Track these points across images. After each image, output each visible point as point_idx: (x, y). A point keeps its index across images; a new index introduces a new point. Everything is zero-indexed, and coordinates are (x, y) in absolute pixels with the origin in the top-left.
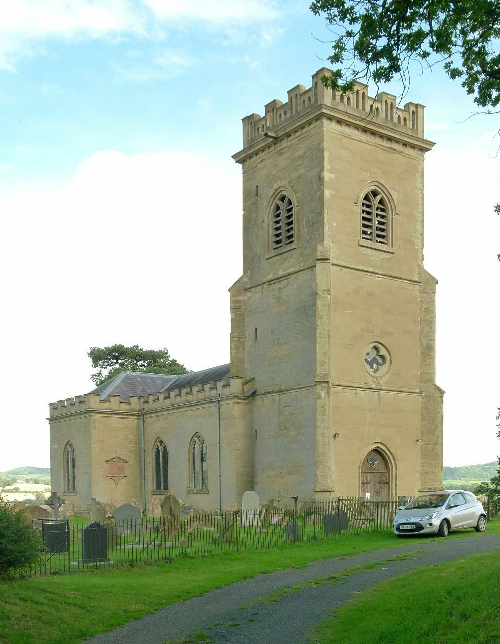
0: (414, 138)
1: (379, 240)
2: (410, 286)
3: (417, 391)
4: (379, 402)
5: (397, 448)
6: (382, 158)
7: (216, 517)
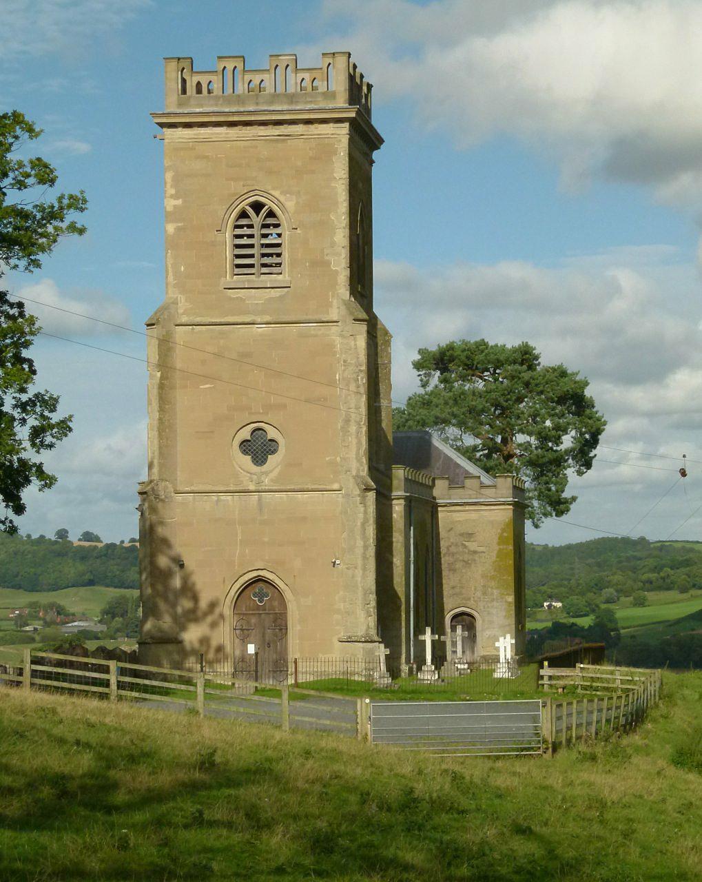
0: (337, 110)
1: (265, 270)
2: (320, 330)
3: (336, 486)
4: (261, 510)
5: (294, 576)
6: (266, 153)
7: (315, 663)
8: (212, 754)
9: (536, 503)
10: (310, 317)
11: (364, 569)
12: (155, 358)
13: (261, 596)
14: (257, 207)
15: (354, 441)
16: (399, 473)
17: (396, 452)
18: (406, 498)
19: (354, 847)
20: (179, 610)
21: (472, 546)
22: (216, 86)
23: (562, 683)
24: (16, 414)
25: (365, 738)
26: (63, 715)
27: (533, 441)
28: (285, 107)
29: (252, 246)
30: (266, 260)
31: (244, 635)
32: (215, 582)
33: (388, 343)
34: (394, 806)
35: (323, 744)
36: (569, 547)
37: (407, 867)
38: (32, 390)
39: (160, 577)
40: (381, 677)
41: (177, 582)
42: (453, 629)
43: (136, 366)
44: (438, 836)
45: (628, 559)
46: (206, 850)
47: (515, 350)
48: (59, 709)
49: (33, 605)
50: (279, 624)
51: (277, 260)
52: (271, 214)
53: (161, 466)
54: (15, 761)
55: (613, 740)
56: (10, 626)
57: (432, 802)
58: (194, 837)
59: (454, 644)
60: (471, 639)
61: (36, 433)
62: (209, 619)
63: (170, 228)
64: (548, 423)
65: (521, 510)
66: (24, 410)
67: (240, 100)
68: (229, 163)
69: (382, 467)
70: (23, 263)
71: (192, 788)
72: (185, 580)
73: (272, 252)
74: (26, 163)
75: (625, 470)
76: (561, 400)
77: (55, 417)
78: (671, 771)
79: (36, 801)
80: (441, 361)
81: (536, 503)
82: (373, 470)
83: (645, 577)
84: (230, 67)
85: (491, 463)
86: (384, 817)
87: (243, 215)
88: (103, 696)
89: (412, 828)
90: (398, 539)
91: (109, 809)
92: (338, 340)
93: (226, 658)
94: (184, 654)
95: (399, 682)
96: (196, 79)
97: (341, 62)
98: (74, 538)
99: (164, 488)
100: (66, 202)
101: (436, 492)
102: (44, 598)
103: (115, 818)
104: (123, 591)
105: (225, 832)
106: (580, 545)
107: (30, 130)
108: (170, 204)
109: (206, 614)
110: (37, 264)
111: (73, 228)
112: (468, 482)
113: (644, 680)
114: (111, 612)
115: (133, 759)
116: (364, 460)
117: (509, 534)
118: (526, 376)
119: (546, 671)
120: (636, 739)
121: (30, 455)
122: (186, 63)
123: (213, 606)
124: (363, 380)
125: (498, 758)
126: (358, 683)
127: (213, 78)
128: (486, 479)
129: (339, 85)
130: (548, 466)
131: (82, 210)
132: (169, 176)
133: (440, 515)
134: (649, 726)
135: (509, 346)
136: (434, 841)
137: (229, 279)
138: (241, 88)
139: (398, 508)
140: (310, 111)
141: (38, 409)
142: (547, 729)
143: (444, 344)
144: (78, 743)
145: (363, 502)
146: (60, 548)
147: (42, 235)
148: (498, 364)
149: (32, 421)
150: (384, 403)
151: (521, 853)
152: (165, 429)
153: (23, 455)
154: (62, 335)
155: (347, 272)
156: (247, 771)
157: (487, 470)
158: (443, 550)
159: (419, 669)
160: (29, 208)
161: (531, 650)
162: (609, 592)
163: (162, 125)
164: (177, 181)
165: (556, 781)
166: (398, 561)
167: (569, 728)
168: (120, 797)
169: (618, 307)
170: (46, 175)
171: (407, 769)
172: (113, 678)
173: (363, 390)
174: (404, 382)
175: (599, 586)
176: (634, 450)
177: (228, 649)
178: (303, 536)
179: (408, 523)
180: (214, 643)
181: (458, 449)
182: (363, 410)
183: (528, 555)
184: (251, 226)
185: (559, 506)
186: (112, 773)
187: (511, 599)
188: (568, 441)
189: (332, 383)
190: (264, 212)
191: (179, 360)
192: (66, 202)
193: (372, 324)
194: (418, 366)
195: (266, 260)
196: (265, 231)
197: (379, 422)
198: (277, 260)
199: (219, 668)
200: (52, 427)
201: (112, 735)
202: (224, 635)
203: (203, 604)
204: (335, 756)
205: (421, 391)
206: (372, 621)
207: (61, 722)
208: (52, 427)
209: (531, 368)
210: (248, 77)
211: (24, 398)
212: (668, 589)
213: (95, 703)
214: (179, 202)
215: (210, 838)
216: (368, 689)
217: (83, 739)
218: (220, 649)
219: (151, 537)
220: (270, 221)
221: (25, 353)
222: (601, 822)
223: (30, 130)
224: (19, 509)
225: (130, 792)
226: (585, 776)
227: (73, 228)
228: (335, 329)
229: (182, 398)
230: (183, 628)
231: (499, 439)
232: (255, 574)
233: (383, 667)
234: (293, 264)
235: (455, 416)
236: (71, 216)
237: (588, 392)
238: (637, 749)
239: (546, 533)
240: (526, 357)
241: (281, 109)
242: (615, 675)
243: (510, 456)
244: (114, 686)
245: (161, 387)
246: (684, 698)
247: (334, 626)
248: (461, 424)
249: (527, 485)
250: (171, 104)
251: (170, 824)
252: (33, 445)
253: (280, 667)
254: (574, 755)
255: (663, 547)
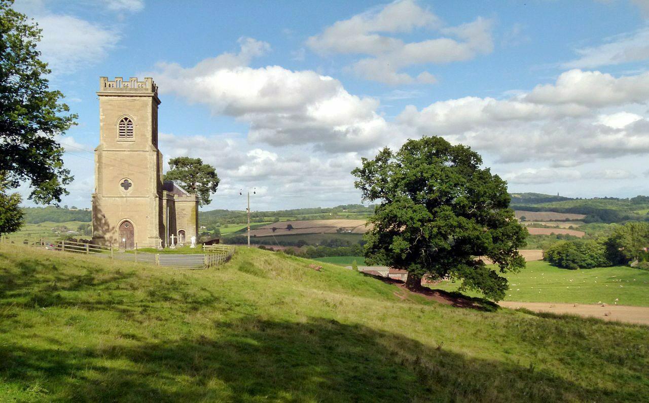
3: (148, 196)
8: (119, 270)
9: (201, 201)
10: (141, 150)
11: (155, 218)
12: (97, 160)
13: (127, 225)
14: (126, 119)
15: (153, 184)
16: (165, 193)
17: (164, 187)
18: (167, 200)
19: (160, 295)
20: (104, 229)
21: (184, 212)
22: (115, 85)
23: (208, 249)
24: (58, 174)
25: (157, 265)
26: (76, 259)
27: (201, 184)
28: (134, 92)
29: (124, 130)
30: (128, 134)
31: (122, 237)
32: (114, 221)
33: (162, 157)
34: (170, 283)
35: (147, 266)
36: (208, 212)
37: (175, 300)
38: (63, 168)
39: (98, 220)
40: (160, 247)
41: (103, 221)
42: (179, 234)
43: (91, 161)
44: (182, 291)
45: (223, 215)
46: (121, 296)
47: (196, 160)
48: (74, 257)
49: (58, 226)
50: (132, 233)
51: (132, 134)
52: (130, 121)
53: (98, 190)
54: (65, 272)
55: (223, 264)
56: (51, 232)
57: (179, 282)
58: (116, 293)
59: (179, 239)
60: (184, 237)
61: (64, 180)
62: (112, 232)
63: (101, 124)
64: (205, 180)
65: (197, 203)
66: (61, 174)
67: (121, 89)
68: (119, 107)
69: (160, 191)
70: (61, 133)
71: (115, 279)
72: (106, 221)
73: (130, 131)
74: (61, 105)
75: (226, 191)
76: (208, 174)
77: (69, 176)
78: (239, 272)
79: (73, 283)
80: (176, 162)
81: (201, 201)
82: (158, 192)
83: (227, 220)
84: (119, 80)
85: (189, 190)
86: (167, 286)
87: (122, 121)
88: (85, 253)
89: (176, 289)
90: (164, 210)
91: (94, 285)
92: (148, 156)
93: (117, 242)
94: (105, 241)
95: (165, 249)
96: (109, 83)
97: (150, 80)
98: (70, 208)
99: (99, 196)
100: (72, 116)
101: (174, 198)
102: (61, 224)
103: (96, 287)
104: (83, 223)
105: (126, 291)
106: (211, 211)
107: (62, 96)
108: (101, 117)
109: (111, 230)
110: (64, 133)
111: (74, 123)
112: (183, 195)
113: (230, 248)
114: (80, 228)
115: (97, 271)
116: (156, 189)
117: (194, 210)
118: (199, 167)
119: (205, 246)
120: (228, 264)
121: (62, 186)
122: (106, 79)
123: (113, 228)
124: (155, 167)
125: (194, 269)
126: (154, 249)
127: (114, 83)
128: (188, 194)
129: (149, 87)
130: (205, 191)
131: (77, 118)
132: (101, 110)
133: (176, 204)
134: (232, 260)
135: (194, 159)
136: (181, 292)
137: (118, 139)
138: (122, 86)
139: (165, 202)
140: (121, 93)
141: (64, 173)
142: (206, 262)
143: (177, 158)
144: (82, 267)
145: (155, 200)
146: (66, 211)
147: (65, 125)
148: (192, 164)
149: (63, 177)
150: (161, 173)
151: (204, 295)
152: (100, 180)
153: (61, 186)
154: (74, 152)
155: (151, 138)
156: (128, 274)
157: (188, 192)
158: (176, 214)
159: (170, 245)
160: (61, 117)
161: (198, 242)
162: (218, 224)
163: (99, 95)
164: (103, 111)
165: (210, 276)
166: (164, 216)
167: (212, 261)
168: (95, 282)
169: (228, 149)
170: (67, 108)
171: (171, 273)
172: (88, 249)
173: (155, 170)
174: (166, 168)
175: (215, 222)
176: (227, 186)
177: (118, 240)
178: (141, 208)
179: (167, 206)
180: (114, 238)
181: (180, 186)
182: (155, 176)
183: (199, 214)
184: (124, 124)
185: (207, 202)
186: (92, 275)
187: (195, 227)
188: (210, 185)
189: (147, 168)
190: (128, 121)
191: (104, 160)
192: (72, 116)
193: (158, 152)
194: (169, 163)
195: (128, 134)
196: (128, 126)
197: (160, 179)
198: (132, 134)
199: (115, 245)
200: (68, 178)
201: (90, 264)
202: (117, 236)
203: (111, 227)
204: (151, 270)
205: (171, 170)
206: (157, 232)
207: (76, 261)
208: (68, 178)
209: (200, 165)
210: (124, 83)
211: (60, 170)
212: (234, 223)
213: (83, 255)
214: (104, 117)
215: (122, 292)
216: (157, 251)
217: (83, 266)
218: (115, 240)
219: (96, 209)
220: (129, 123)
221: (61, 158)
222: (223, 286)
223: (62, 96)
224: (59, 201)
225: (98, 280)
226: (217, 274)
227: (74, 123)
228: (148, 153)
229: (105, 172)
230: (105, 234)
231: (191, 184)
232: (125, 220)
233: (161, 245)
234: (136, 135)
235: (180, 177)
236: (74, 120)
237: (215, 172)
238: (229, 267)
239: (204, 208)
240: (199, 162)
241: (133, 92)
242: (222, 246)
243: (194, 189)
244: (88, 250)
245: (99, 168)
246: (241, 253)
247: (147, 234)
248: (181, 180)
249: (199, 196)
250: (102, 89)
251: (110, 289)
252: (63, 183)
253: (132, 245)
254: (214, 268)
255: (233, 212)
